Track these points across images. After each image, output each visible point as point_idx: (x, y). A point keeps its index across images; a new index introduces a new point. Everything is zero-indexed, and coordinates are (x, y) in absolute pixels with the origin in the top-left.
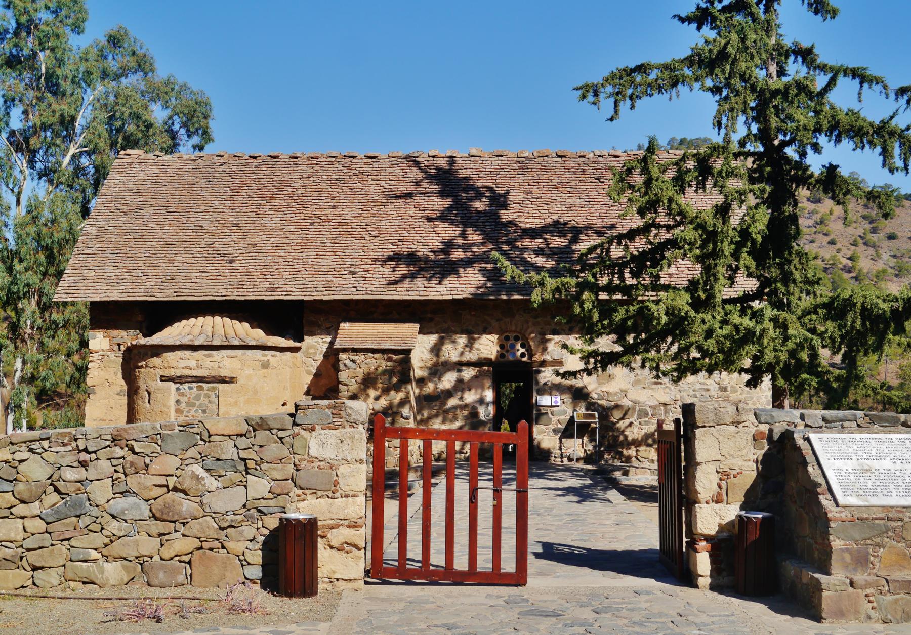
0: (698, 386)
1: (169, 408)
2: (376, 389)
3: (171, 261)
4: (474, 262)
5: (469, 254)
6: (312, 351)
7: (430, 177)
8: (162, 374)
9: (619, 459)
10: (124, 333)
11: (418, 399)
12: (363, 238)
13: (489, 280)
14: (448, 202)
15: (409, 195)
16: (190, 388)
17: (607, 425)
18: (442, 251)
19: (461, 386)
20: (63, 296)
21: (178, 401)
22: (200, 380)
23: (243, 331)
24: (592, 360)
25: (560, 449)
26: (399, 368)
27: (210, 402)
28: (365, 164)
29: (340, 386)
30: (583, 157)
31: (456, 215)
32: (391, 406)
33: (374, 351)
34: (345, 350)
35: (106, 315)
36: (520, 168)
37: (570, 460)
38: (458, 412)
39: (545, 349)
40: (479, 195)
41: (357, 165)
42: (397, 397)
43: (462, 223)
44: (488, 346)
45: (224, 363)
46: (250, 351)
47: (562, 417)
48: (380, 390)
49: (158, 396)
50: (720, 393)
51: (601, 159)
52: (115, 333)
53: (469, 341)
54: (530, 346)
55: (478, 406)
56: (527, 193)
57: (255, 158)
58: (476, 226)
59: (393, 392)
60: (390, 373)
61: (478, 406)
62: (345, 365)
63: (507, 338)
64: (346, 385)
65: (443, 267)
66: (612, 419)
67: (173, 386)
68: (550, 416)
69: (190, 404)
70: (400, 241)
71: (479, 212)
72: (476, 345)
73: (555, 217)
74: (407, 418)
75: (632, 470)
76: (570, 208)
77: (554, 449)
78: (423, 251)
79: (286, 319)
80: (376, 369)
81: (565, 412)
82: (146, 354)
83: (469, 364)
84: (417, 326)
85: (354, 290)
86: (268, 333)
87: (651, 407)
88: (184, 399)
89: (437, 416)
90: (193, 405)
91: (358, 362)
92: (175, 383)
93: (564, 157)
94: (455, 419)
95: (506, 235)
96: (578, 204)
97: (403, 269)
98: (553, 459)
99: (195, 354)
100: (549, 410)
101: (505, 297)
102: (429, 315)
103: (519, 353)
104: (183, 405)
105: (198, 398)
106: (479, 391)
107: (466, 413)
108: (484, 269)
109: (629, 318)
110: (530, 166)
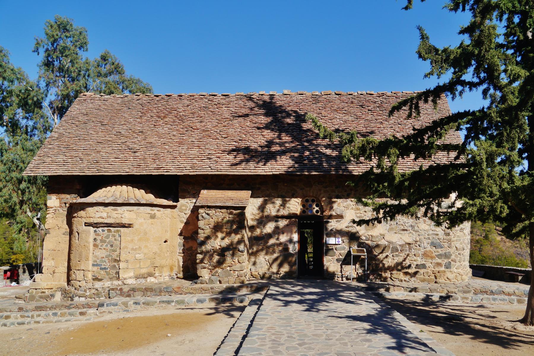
0: (431, 232)
1: (89, 243)
2: (222, 232)
3: (99, 152)
4: (287, 152)
5: (283, 148)
6: (184, 208)
7: (260, 107)
8: (85, 221)
9: (379, 279)
10: (68, 196)
11: (250, 239)
12: (218, 139)
13: (296, 163)
14: (269, 119)
15: (247, 115)
16: (103, 231)
17: (372, 257)
18: (266, 146)
19: (277, 231)
20: (29, 172)
21: (95, 239)
22: (109, 225)
23: (140, 195)
24: (382, 211)
25: (341, 272)
26: (237, 219)
27: (115, 240)
28: (221, 99)
29: (199, 230)
30: (351, 95)
31: (275, 126)
32: (232, 244)
33: (221, 208)
34: (202, 207)
35: (57, 184)
36: (313, 100)
37: (347, 279)
38: (276, 248)
39: (331, 208)
40: (288, 115)
41: (216, 100)
42: (236, 238)
43: (278, 130)
44: (295, 206)
45: (125, 214)
46: (142, 207)
47: (343, 252)
48: (225, 233)
49: (83, 235)
50: (445, 237)
51: (362, 96)
52: (63, 196)
53: (283, 203)
54: (322, 206)
55: (288, 244)
56: (319, 114)
57: (157, 96)
58: (287, 132)
59: (233, 235)
60: (231, 222)
61: (288, 244)
62: (203, 217)
63: (307, 201)
64: (203, 229)
65: (267, 155)
66: (375, 253)
67: (92, 229)
68: (335, 250)
69: (102, 241)
70: (240, 140)
71: (289, 124)
72: (287, 205)
73: (337, 127)
74: (242, 252)
75: (391, 287)
76: (345, 122)
77: (337, 272)
78: (254, 146)
79: (167, 187)
80: (223, 220)
81: (344, 248)
82: (78, 209)
83: (283, 217)
84: (250, 192)
85: (210, 168)
86: (156, 197)
87: (400, 245)
88: (99, 238)
89: (262, 250)
90: (105, 242)
91: (211, 214)
92: (93, 227)
93: (340, 94)
94: (274, 252)
95: (306, 137)
96: (350, 120)
97: (241, 157)
98: (336, 278)
99: (106, 209)
100: (334, 247)
101: (306, 173)
102: (257, 186)
103: (314, 211)
104: (98, 242)
105: (107, 237)
106: (289, 234)
107: (281, 248)
108: (293, 156)
109: (406, 180)
110: (320, 99)
